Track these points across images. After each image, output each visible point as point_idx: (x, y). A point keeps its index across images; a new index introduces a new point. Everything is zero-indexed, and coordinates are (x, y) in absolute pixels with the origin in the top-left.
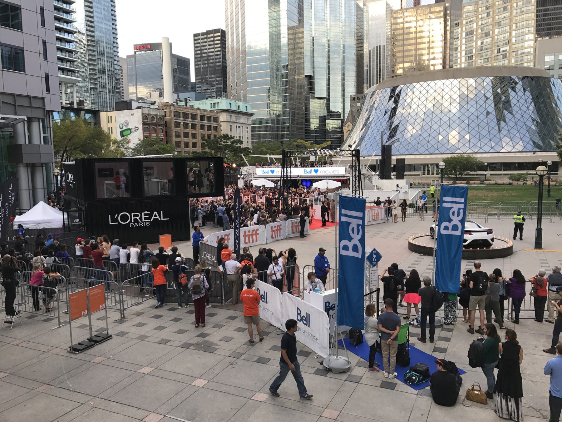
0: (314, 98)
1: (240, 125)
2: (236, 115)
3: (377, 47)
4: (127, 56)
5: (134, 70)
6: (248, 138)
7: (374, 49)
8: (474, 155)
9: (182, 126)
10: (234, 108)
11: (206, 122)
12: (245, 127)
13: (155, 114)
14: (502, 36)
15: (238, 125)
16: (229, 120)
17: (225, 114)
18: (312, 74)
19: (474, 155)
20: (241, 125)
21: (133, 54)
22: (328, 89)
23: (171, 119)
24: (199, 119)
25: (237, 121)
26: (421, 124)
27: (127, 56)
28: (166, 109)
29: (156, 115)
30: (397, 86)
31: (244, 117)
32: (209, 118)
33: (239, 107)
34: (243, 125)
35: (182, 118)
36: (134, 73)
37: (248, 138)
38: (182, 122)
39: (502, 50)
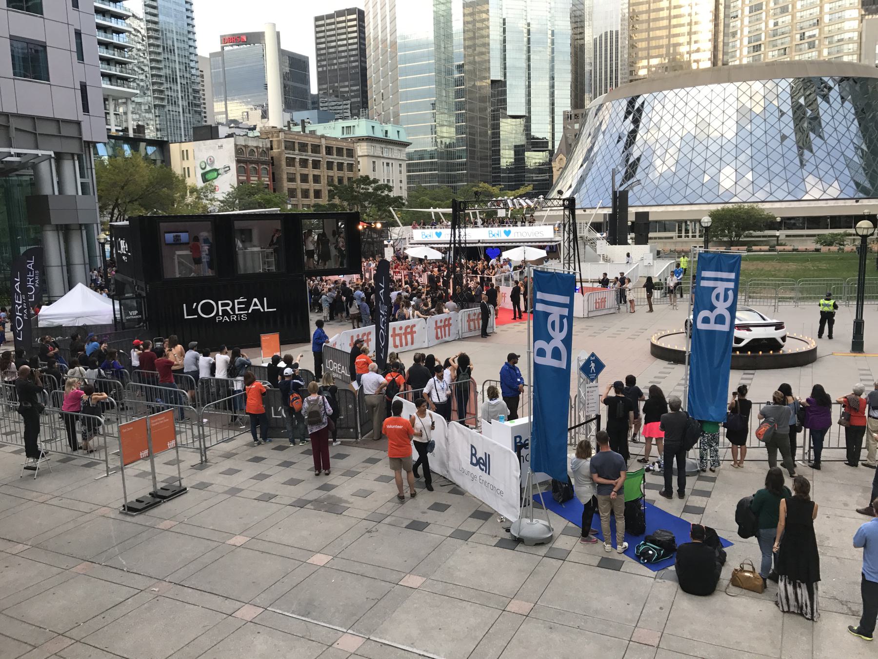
0: (506, 117)
1: (388, 161)
2: (383, 146)
3: (606, 33)
4: (211, 54)
5: (222, 77)
6: (401, 181)
7: (601, 37)
8: (760, 206)
9: (297, 164)
10: (379, 134)
11: (335, 156)
12: (396, 164)
13: (255, 145)
14: (809, 12)
15: (386, 161)
16: (372, 154)
17: (365, 144)
18: (502, 79)
19: (760, 206)
20: (390, 162)
21: (220, 50)
22: (529, 102)
23: (280, 154)
25: (385, 155)
26: (676, 157)
27: (211, 54)
28: (272, 137)
29: (257, 147)
30: (638, 96)
31: (396, 148)
32: (340, 151)
33: (386, 132)
35: (297, 152)
36: (222, 81)
37: (401, 181)
39: (807, 34)
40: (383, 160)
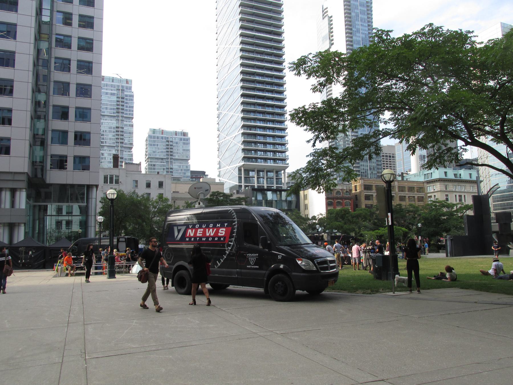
5: (402, 156)
11: (407, 193)
13: (341, 188)
17: (438, 184)
23: (360, 192)
24: (397, 190)
29: (342, 190)
31: (468, 185)
33: (460, 175)
34: (466, 194)
38: (416, 196)
40: (455, 194)
